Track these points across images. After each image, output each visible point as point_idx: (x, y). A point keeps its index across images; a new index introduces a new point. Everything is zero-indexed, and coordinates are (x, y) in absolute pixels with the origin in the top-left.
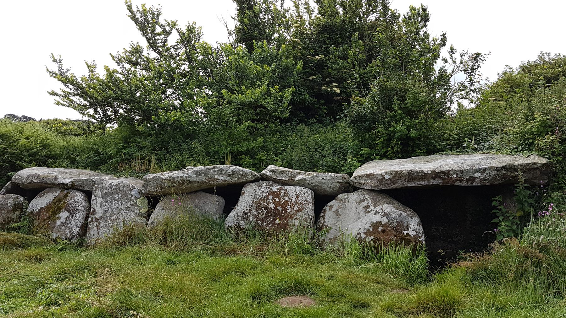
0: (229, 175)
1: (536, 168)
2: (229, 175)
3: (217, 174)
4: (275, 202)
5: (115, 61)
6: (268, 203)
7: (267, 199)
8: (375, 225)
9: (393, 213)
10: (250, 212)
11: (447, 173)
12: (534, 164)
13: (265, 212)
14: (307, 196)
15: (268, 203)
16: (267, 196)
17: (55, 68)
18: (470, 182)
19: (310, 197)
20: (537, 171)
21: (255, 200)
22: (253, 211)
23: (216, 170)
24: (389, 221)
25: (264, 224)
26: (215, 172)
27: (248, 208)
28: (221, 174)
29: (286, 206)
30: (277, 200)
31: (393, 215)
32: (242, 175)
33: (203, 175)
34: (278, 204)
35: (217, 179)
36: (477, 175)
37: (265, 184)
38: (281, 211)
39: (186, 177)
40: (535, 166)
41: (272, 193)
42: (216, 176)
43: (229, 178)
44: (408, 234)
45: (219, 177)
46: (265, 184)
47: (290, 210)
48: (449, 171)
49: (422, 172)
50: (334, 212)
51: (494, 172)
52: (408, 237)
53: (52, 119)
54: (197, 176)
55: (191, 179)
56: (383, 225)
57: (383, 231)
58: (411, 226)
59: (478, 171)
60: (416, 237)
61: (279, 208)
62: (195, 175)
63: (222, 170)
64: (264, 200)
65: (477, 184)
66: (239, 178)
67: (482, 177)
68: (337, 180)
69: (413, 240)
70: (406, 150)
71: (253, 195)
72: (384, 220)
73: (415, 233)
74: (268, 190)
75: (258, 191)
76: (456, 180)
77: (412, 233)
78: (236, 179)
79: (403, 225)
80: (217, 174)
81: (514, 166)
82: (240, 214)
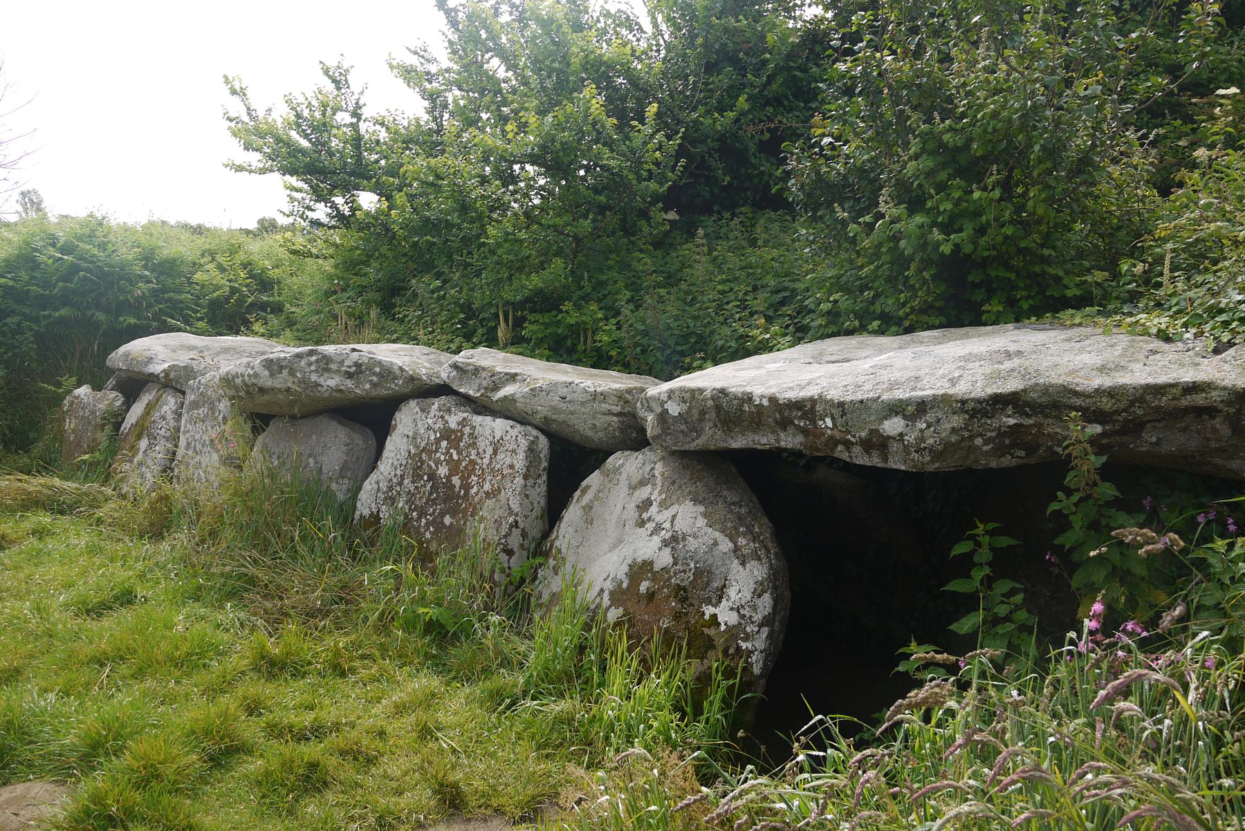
0: (349, 375)
1: (1210, 411)
2: (349, 375)
3: (316, 371)
4: (450, 461)
5: (330, 77)
6: (438, 462)
7: (436, 451)
8: (640, 570)
9: (695, 536)
10: (400, 484)
11: (806, 409)
12: (1194, 388)
13: (428, 488)
14: (504, 446)
15: (438, 462)
16: (438, 441)
17: (237, 108)
18: (875, 454)
19: (521, 456)
20: (1217, 422)
21: (413, 452)
22: (406, 481)
23: (314, 358)
24: (675, 564)
25: (423, 520)
26: (310, 365)
27: (399, 472)
28: (328, 370)
29: (469, 477)
30: (455, 457)
31: (692, 544)
32: (380, 375)
33: (285, 372)
34: (454, 467)
35: (317, 385)
36: (893, 426)
37: (436, 405)
38: (457, 489)
39: (249, 375)
40: (1199, 399)
41: (447, 434)
42: (314, 377)
43: (350, 383)
44: (714, 617)
45: (321, 381)
46: (436, 405)
47: (475, 490)
48: (813, 401)
49: (749, 398)
50: (584, 508)
51: (957, 421)
52: (711, 632)
53: (208, 226)
54: (272, 375)
55: (261, 382)
56: (655, 577)
57: (651, 596)
58: (732, 592)
59: (895, 408)
60: (734, 633)
61: (456, 480)
62: (267, 373)
63: (327, 359)
64: (430, 452)
65: (896, 464)
66: (374, 385)
67: (910, 438)
68: (605, 406)
69: (720, 642)
70: (963, 296)
71: (411, 434)
72: (664, 559)
73: (733, 619)
74: (440, 425)
75: (420, 424)
76: (834, 442)
77: (726, 615)
78: (368, 386)
79: (708, 584)
80: (316, 371)
81: (1076, 394)
82: (384, 486)
